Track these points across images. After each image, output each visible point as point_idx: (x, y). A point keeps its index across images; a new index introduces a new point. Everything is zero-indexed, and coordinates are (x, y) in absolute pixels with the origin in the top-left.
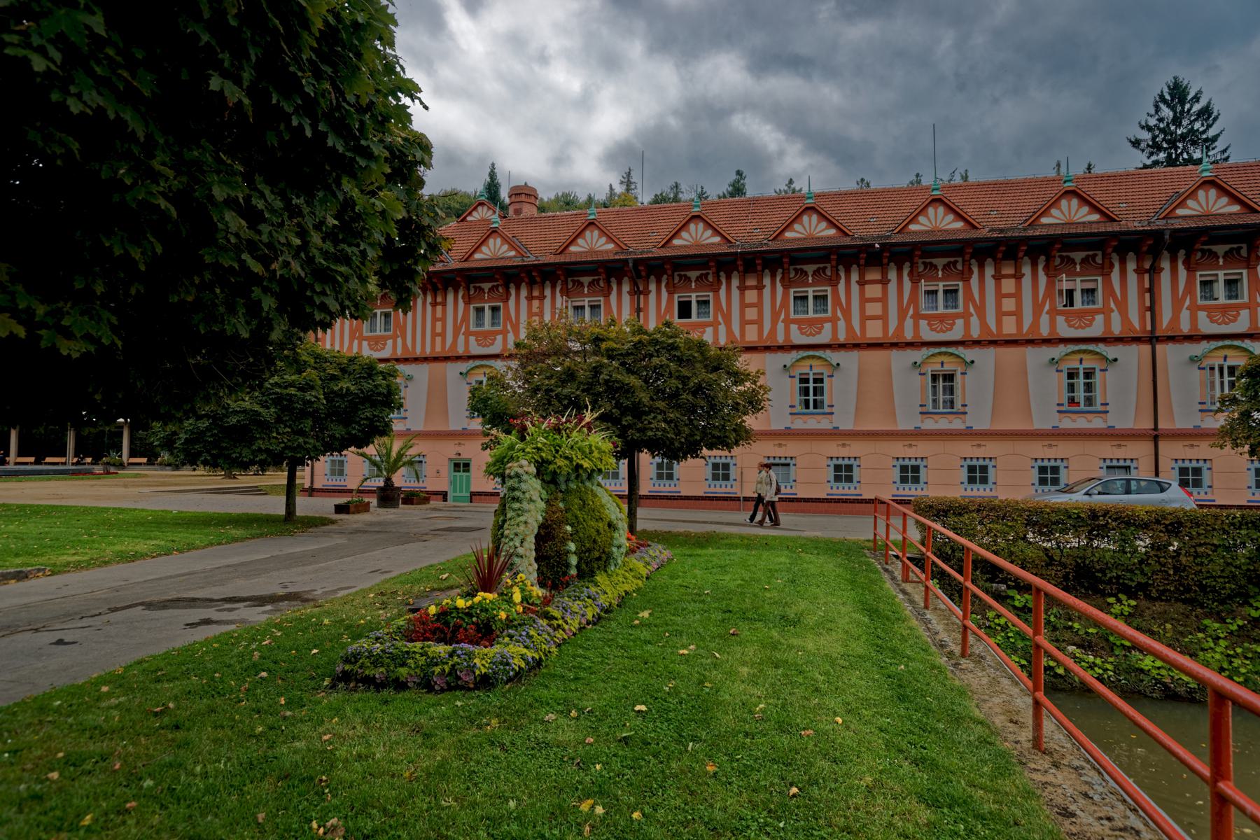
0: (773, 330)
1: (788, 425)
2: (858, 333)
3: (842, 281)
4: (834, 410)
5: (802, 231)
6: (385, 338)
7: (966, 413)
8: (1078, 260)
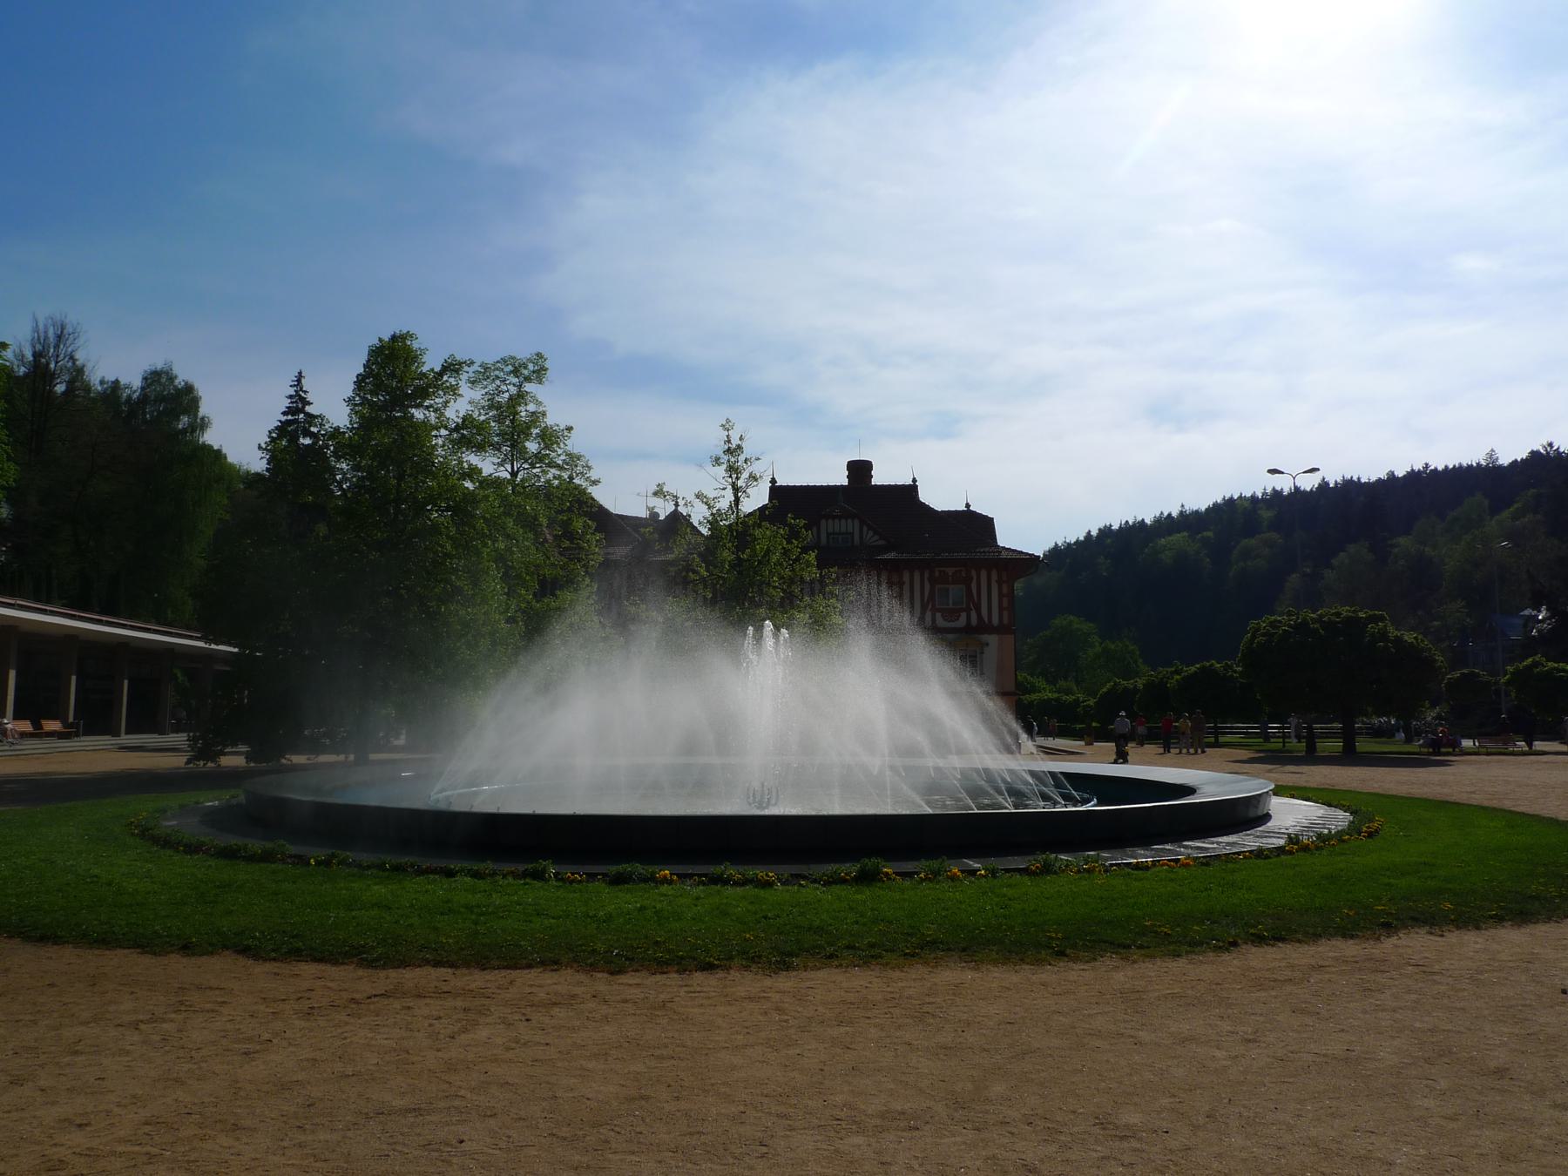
2: (986, 620)
5: (868, 537)
8: (950, 574)
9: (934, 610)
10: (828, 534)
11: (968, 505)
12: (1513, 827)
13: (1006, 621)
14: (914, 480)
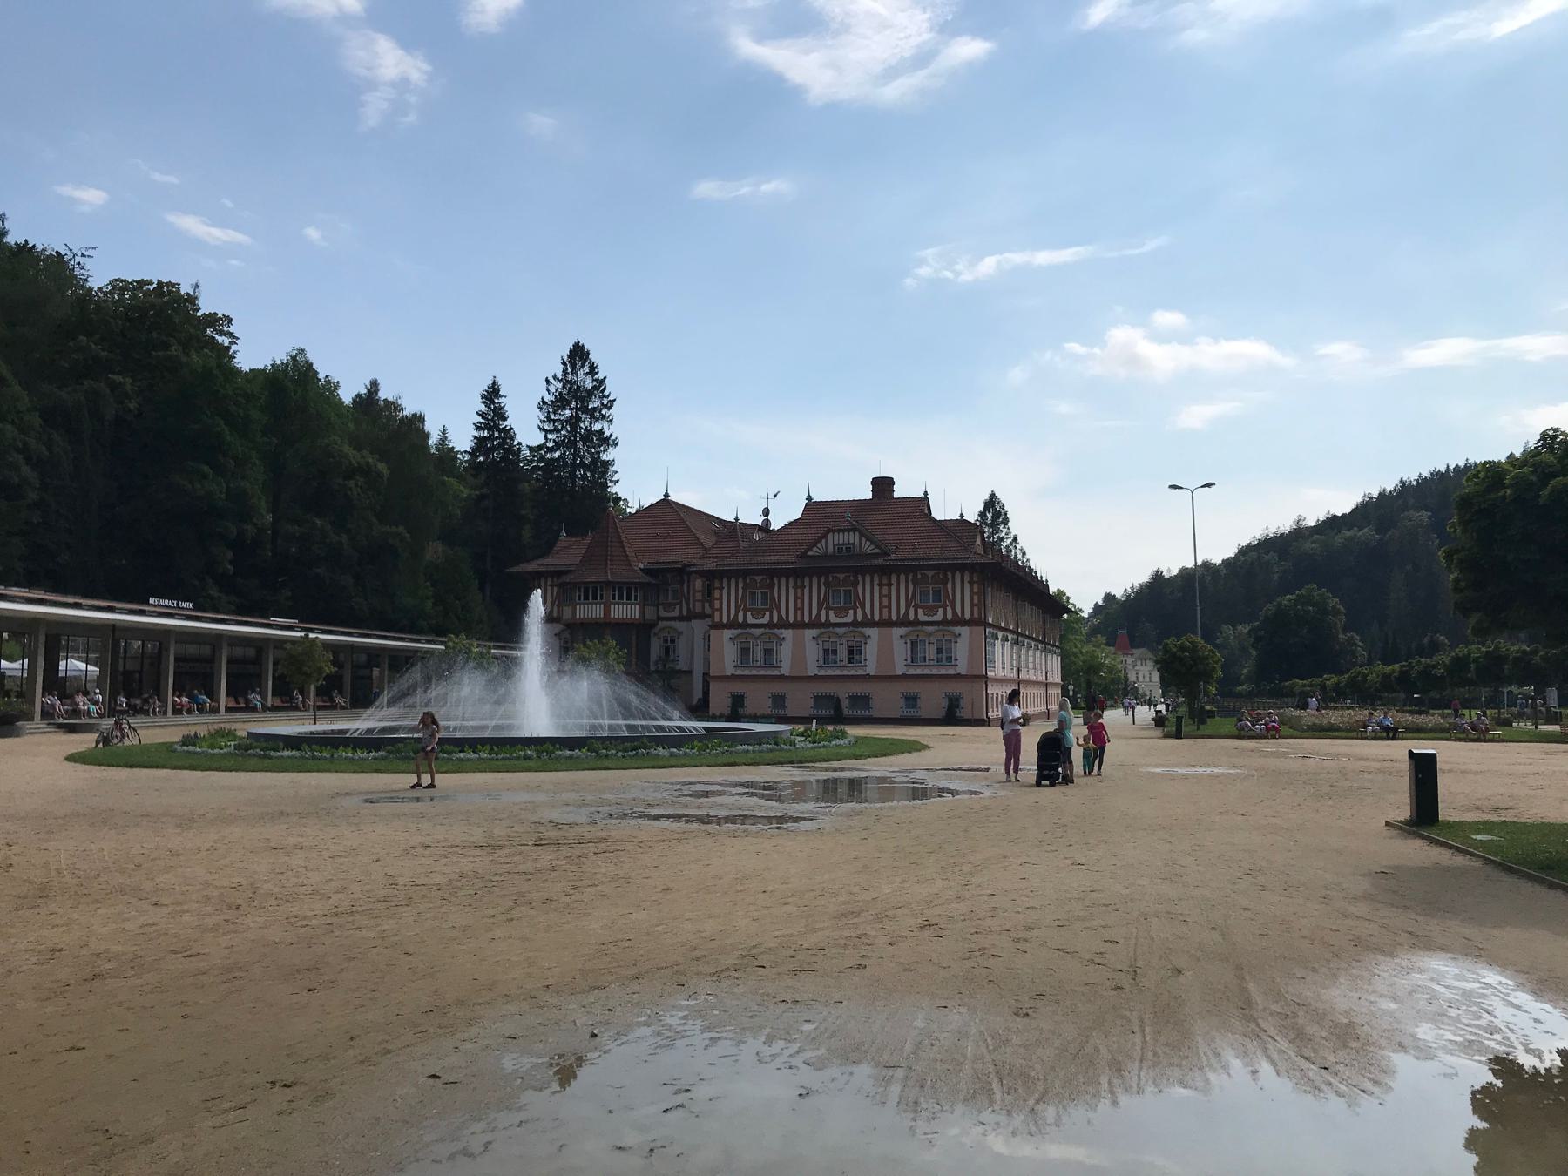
0: (818, 615)
1: (733, 672)
2: (960, 615)
3: (860, 585)
4: (958, 663)
5: (818, 551)
6: (847, 609)
7: (866, 666)
8: (930, 576)
9: (745, 610)
10: (834, 545)
11: (962, 516)
13: (976, 615)
14: (926, 493)
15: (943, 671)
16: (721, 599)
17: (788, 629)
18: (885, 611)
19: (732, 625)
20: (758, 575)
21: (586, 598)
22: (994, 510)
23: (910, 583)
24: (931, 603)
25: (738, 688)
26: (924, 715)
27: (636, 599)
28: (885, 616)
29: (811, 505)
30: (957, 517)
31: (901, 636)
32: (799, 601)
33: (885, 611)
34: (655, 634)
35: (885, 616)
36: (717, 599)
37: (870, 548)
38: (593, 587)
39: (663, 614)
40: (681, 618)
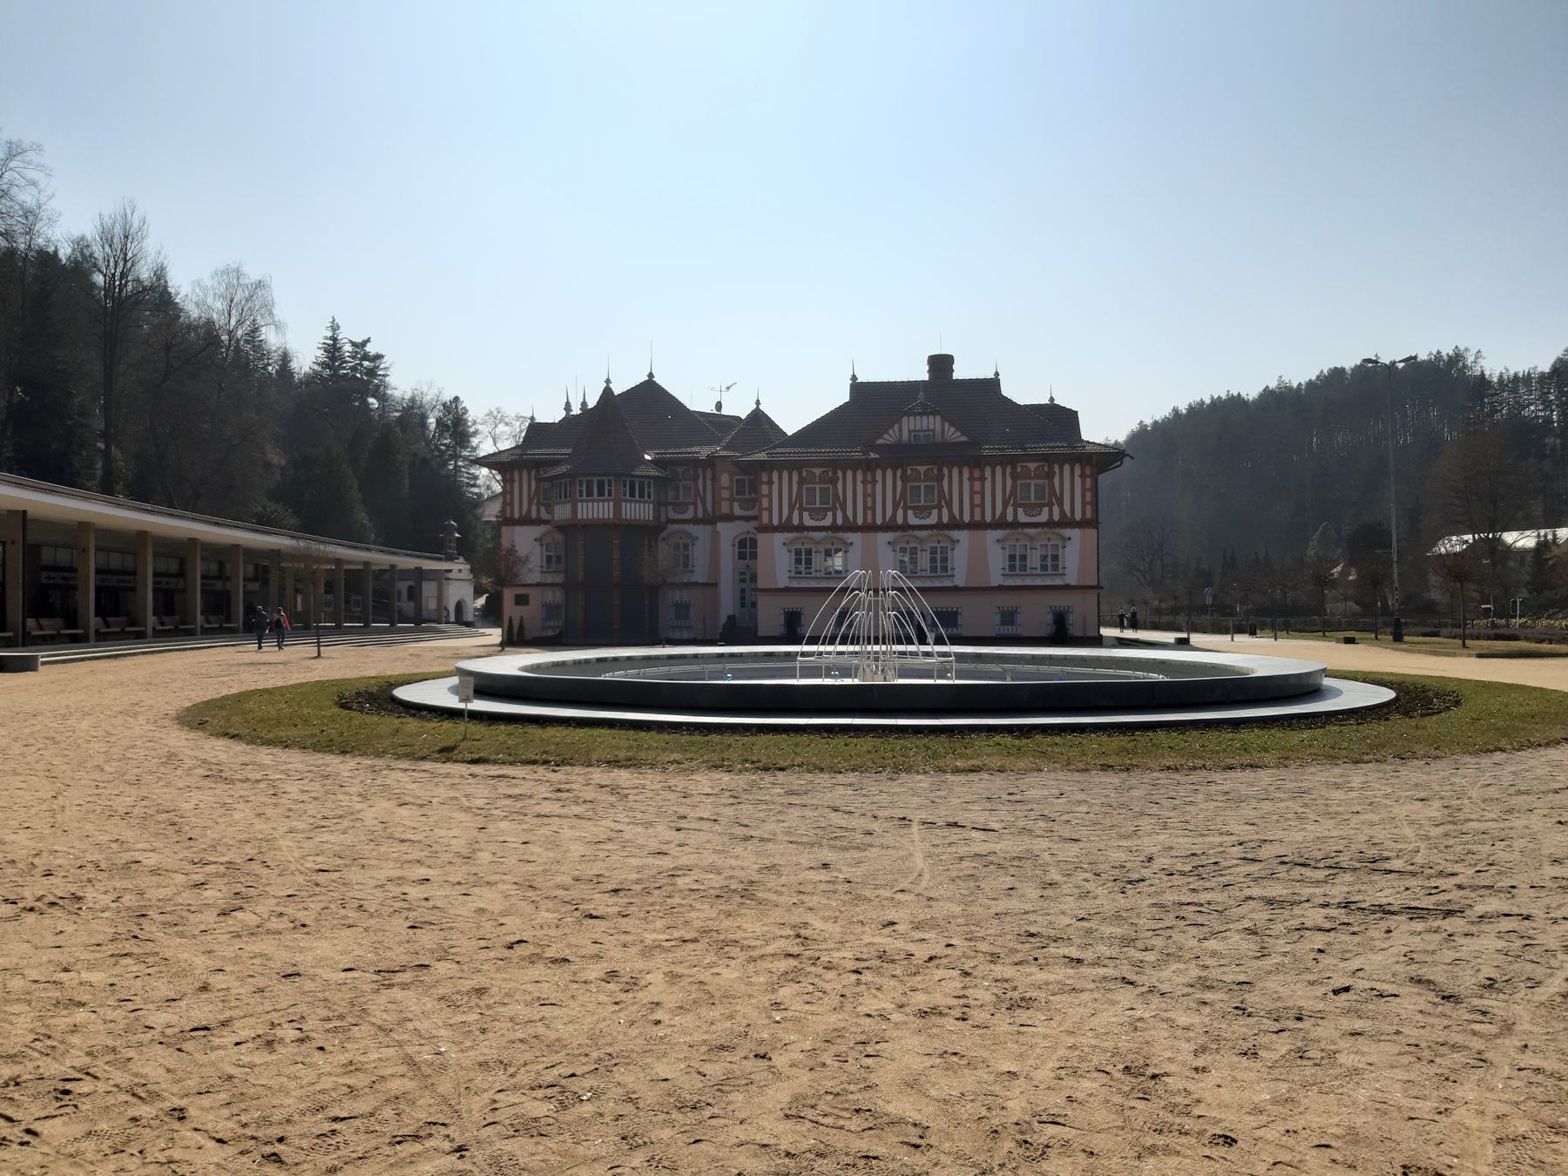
2: (1068, 514)
4: (1066, 571)
10: (910, 432)
11: (1052, 399)
12: (1407, 889)
13: (1088, 516)
14: (997, 374)
15: (1048, 582)
16: (770, 496)
17: (857, 532)
18: (977, 511)
19: (786, 527)
20: (1033, 461)
21: (632, 494)
22: (456, 399)
23: (533, 480)
24: (922, 503)
25: (792, 603)
26: (1025, 634)
27: (649, 497)
28: (869, 520)
29: (858, 389)
30: (1046, 401)
31: (998, 541)
32: (869, 499)
33: (977, 511)
34: (664, 539)
35: (977, 517)
36: (765, 496)
37: (954, 436)
38: (598, 481)
39: (673, 515)
40: (695, 521)
